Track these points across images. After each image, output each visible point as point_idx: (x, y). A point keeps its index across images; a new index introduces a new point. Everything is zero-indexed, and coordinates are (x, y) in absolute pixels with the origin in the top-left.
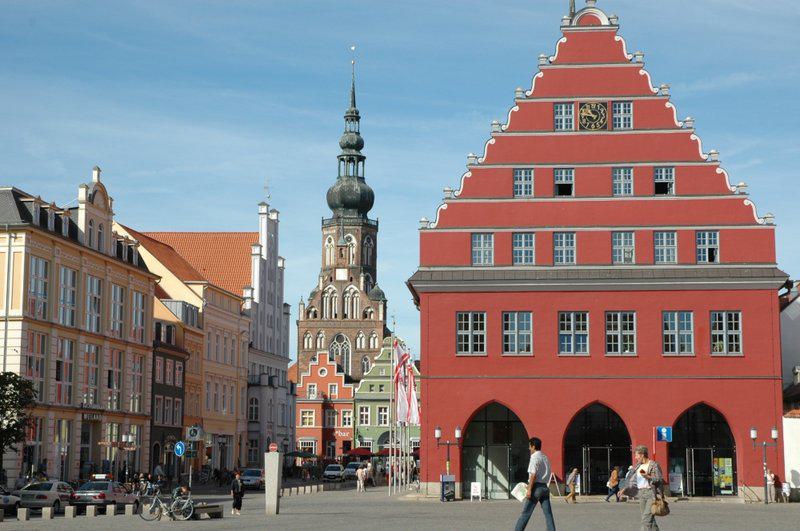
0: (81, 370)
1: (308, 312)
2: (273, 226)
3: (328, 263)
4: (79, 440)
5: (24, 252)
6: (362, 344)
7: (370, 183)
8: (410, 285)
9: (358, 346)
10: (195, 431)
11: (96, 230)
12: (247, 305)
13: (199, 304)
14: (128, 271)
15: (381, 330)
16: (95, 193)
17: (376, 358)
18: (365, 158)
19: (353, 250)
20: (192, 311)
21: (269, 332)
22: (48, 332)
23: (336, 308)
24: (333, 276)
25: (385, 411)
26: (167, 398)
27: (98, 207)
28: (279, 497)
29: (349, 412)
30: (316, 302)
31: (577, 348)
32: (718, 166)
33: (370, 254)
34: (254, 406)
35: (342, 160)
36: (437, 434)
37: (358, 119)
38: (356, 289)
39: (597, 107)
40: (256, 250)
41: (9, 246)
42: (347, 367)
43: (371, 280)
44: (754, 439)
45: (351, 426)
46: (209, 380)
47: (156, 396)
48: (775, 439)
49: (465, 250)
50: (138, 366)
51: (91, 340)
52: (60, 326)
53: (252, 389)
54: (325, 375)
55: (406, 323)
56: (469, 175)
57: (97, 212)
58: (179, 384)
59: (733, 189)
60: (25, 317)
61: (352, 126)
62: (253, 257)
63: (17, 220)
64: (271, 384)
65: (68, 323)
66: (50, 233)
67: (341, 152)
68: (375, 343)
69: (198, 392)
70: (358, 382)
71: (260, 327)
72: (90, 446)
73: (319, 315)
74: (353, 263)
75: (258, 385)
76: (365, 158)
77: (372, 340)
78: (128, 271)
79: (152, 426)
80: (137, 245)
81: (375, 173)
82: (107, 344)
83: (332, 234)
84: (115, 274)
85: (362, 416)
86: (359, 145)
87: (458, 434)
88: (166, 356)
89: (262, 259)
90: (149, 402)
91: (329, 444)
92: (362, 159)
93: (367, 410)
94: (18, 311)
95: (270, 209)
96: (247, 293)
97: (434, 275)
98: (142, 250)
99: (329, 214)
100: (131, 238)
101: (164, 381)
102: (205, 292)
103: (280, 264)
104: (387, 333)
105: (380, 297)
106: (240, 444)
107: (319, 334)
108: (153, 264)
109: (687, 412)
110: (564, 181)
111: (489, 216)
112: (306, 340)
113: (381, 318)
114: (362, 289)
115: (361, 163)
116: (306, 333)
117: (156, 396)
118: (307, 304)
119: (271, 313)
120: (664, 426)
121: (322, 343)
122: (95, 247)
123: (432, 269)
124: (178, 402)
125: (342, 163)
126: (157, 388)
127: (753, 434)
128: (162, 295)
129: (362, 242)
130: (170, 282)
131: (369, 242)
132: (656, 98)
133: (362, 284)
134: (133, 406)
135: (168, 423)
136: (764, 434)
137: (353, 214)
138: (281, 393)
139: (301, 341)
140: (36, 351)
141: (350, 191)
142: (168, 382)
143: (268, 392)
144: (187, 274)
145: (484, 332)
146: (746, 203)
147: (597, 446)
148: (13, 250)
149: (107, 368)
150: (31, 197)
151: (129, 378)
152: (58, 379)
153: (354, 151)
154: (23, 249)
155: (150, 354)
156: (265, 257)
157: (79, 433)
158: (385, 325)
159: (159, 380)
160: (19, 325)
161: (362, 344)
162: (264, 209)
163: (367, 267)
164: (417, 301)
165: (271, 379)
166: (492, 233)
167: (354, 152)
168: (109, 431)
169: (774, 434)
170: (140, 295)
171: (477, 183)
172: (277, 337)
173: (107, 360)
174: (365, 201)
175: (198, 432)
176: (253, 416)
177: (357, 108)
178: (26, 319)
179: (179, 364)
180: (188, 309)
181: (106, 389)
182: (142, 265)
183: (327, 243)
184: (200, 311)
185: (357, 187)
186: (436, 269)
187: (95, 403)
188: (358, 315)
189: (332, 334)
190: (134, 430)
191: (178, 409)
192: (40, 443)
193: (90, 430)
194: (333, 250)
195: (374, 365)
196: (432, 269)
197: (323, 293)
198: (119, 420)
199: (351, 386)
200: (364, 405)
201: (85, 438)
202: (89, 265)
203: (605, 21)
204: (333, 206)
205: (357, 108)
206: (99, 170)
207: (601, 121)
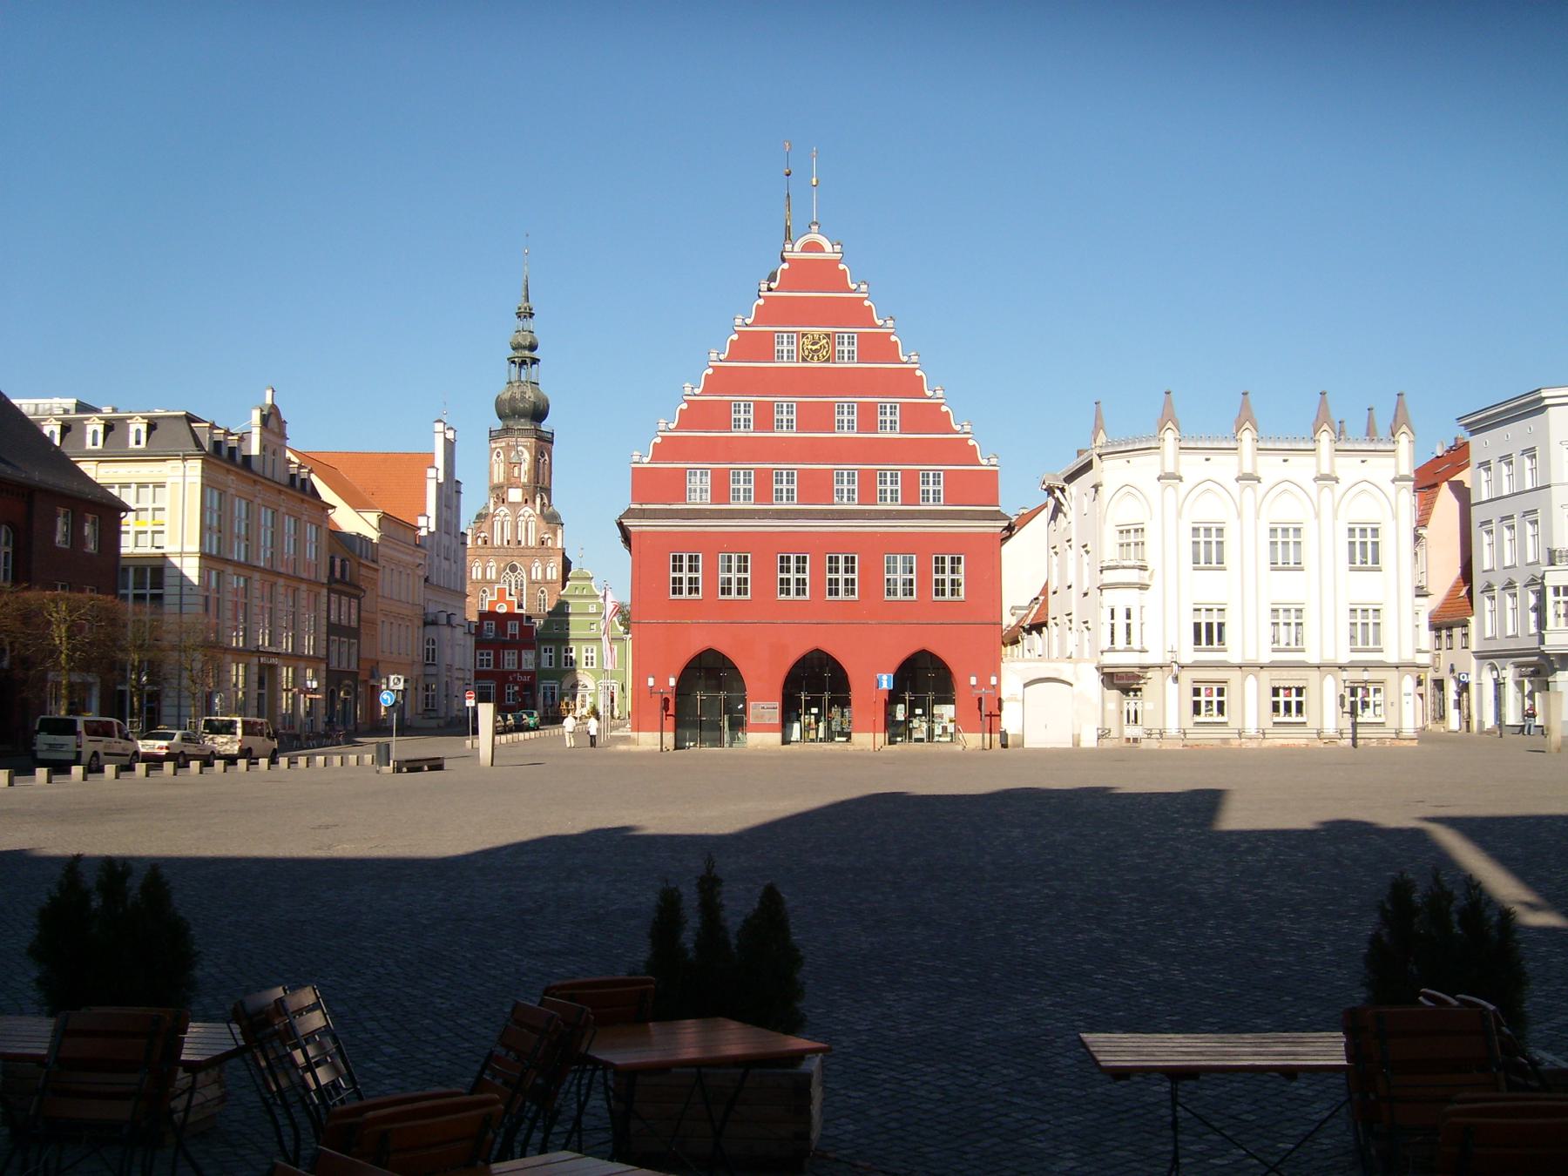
0: (229, 605)
2: (450, 446)
4: (256, 685)
6: (537, 574)
7: (545, 389)
8: (620, 525)
12: (423, 532)
19: (525, 467)
21: (445, 564)
23: (507, 536)
36: (651, 682)
49: (676, 485)
50: (267, 594)
51: (239, 571)
53: (430, 629)
57: (271, 437)
58: (354, 624)
63: (192, 449)
64: (449, 624)
67: (512, 353)
71: (436, 560)
75: (434, 623)
79: (328, 670)
81: (549, 380)
87: (672, 682)
88: (341, 593)
96: (422, 521)
98: (313, 477)
99: (498, 424)
105: (552, 520)
108: (326, 494)
109: (943, 663)
111: (706, 451)
122: (268, 475)
127: (973, 681)
134: (308, 646)
135: (344, 666)
136: (984, 682)
137: (525, 424)
143: (446, 631)
144: (358, 503)
145: (699, 575)
148: (188, 480)
151: (256, 610)
153: (525, 355)
155: (324, 592)
157: (256, 678)
162: (439, 427)
169: (993, 681)
171: (695, 415)
174: (539, 413)
177: (531, 303)
179: (354, 603)
181: (229, 623)
182: (315, 493)
188: (532, 542)
191: (354, 650)
205: (531, 303)
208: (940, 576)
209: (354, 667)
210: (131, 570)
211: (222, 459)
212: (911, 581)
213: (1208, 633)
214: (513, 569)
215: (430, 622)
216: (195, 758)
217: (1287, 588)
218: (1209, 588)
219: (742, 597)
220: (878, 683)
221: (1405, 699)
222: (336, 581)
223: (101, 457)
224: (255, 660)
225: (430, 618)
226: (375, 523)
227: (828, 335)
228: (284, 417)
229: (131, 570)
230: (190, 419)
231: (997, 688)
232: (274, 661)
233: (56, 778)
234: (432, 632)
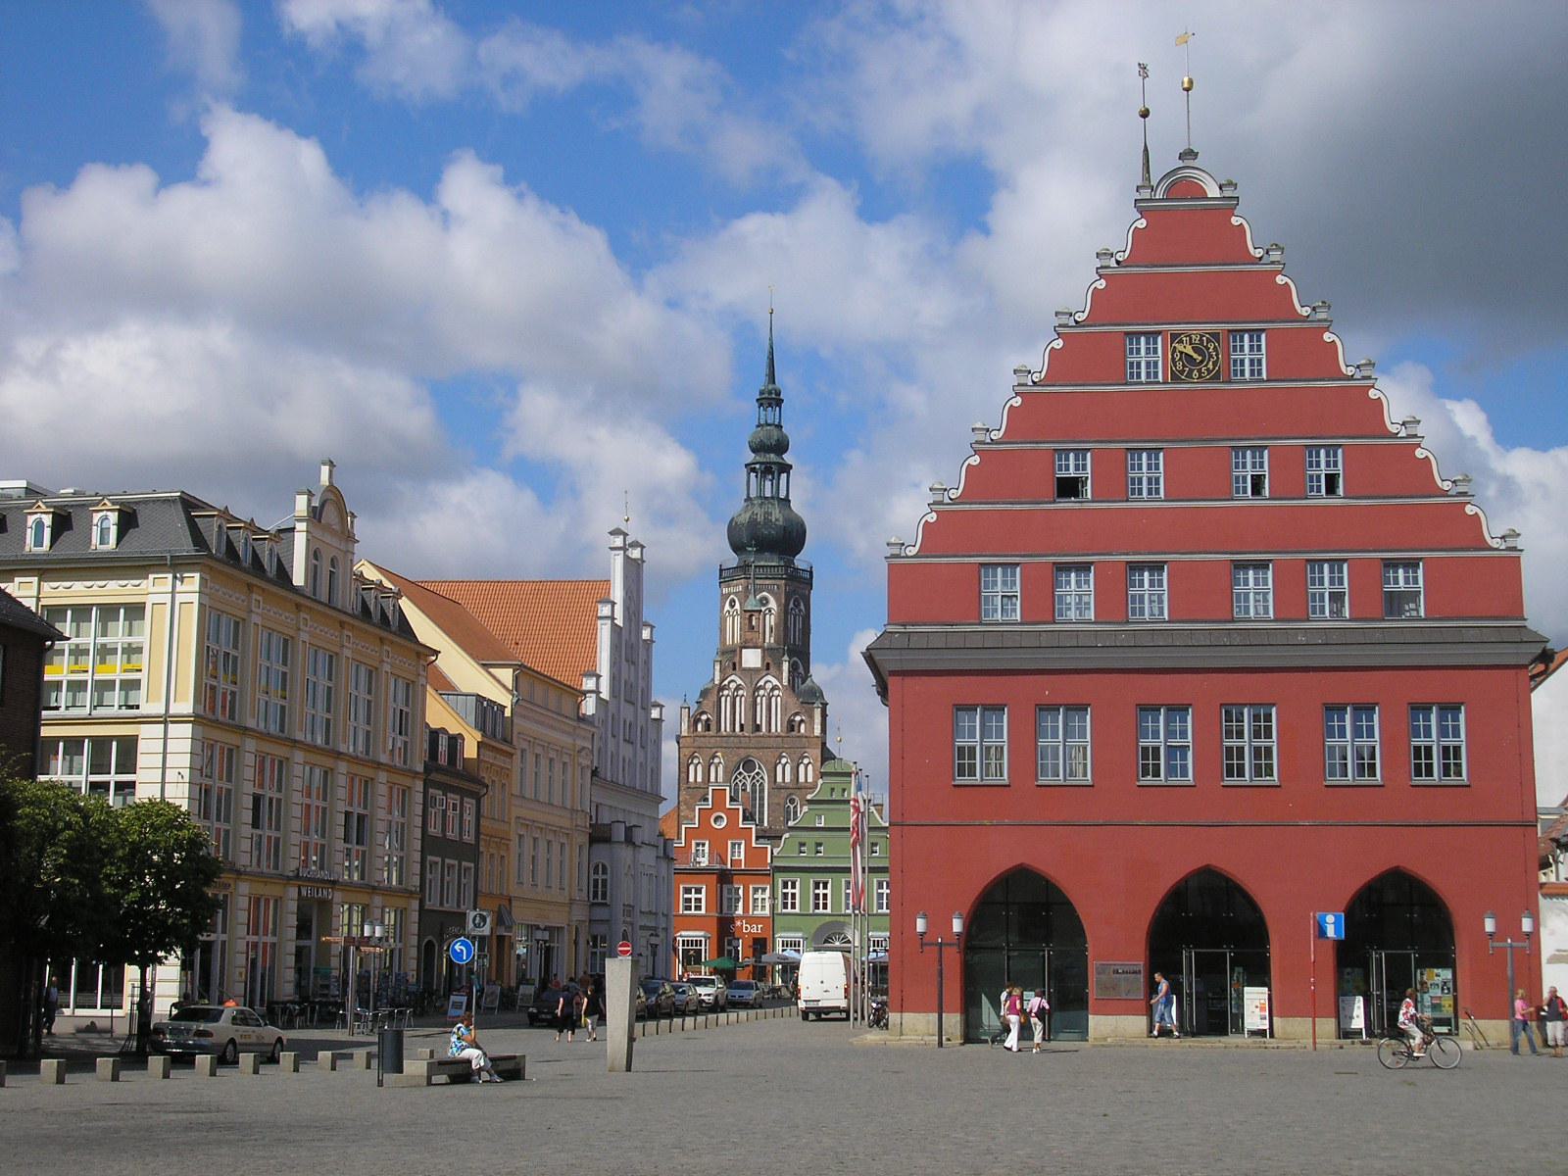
0: (297, 811)
1: (697, 721)
3: (729, 642)
4: (293, 933)
5: (196, 606)
6: (784, 774)
9: (779, 779)
10: (483, 919)
11: (325, 568)
13: (505, 700)
14: (382, 640)
15: (818, 752)
16: (323, 505)
17: (809, 797)
19: (771, 621)
20: (495, 714)
21: (626, 751)
22: (332, 767)
23: (741, 716)
24: (737, 660)
25: (825, 887)
27: (328, 528)
28: (631, 1039)
29: (764, 890)
30: (708, 705)
31: (1171, 771)
32: (1419, 445)
33: (799, 625)
34: (600, 877)
35: (754, 470)
36: (921, 925)
37: (779, 402)
38: (775, 682)
39: (1201, 340)
40: (605, 610)
41: (173, 593)
42: (761, 813)
43: (801, 670)
44: (1491, 935)
45: (767, 912)
46: (550, 837)
47: (429, 858)
48: (1528, 934)
49: (971, 584)
52: (261, 733)
54: (724, 824)
55: (861, 728)
56: (975, 460)
58: (469, 838)
59: (1446, 486)
60: (196, 715)
61: (771, 415)
62: (599, 622)
63: (186, 547)
64: (629, 840)
65: (274, 729)
66: (245, 571)
67: (751, 457)
68: (808, 773)
69: (502, 853)
70: (781, 837)
71: (611, 742)
72: (311, 943)
73: (713, 727)
74: (770, 640)
75: (607, 840)
76: (791, 467)
77: (802, 768)
78: (382, 640)
80: (398, 595)
82: (343, 767)
83: (736, 594)
84: (353, 646)
85: (785, 895)
86: (781, 447)
87: (957, 926)
88: (446, 788)
89: (614, 626)
90: (417, 868)
91: (730, 944)
92: (786, 468)
93: (794, 887)
94: (185, 706)
95: (629, 540)
96: (589, 684)
97: (914, 638)
98: (405, 604)
99: (732, 559)
100: (387, 584)
101: (444, 830)
102: (516, 679)
103: (646, 634)
104: (827, 756)
105: (810, 697)
106: (576, 943)
107: (714, 757)
110: (1072, 473)
112: (692, 768)
113: (817, 731)
114: (785, 683)
116: (692, 757)
118: (694, 707)
119: (630, 718)
120: (1329, 911)
121: (718, 774)
122: (324, 598)
123: (910, 629)
124: (467, 869)
125: (753, 475)
126: (429, 845)
127: (1489, 925)
128: (446, 688)
129: (787, 605)
130: (456, 664)
131: (797, 605)
132: (1306, 325)
133: (785, 675)
135: (447, 907)
138: (647, 856)
139: (684, 770)
140: (267, 785)
141: (767, 521)
142: (449, 834)
143: (625, 854)
144: (486, 654)
146: (1470, 510)
147: (1207, 941)
148: (179, 598)
149: (342, 807)
150: (214, 508)
152: (256, 824)
153: (770, 456)
154: (195, 598)
155: (419, 785)
156: (619, 622)
158: (824, 744)
159: (432, 830)
160: (186, 730)
161: (784, 774)
162: (619, 541)
163: (794, 647)
164: (883, 691)
165: (629, 830)
166: (1018, 564)
167: (772, 457)
168: (345, 921)
169: (1527, 925)
170: (363, 669)
172: (640, 758)
173: (342, 793)
175: (488, 920)
176: (599, 894)
177: (778, 384)
178: (197, 720)
180: (486, 712)
183: (727, 607)
184: (508, 713)
185: (775, 433)
187: (322, 868)
188: (778, 726)
189: (736, 759)
190: (390, 918)
192: (224, 937)
193: (312, 919)
194: (737, 619)
195: (805, 809)
196: (910, 629)
197: (721, 688)
198: (364, 899)
200: (789, 877)
201: (304, 929)
202: (309, 632)
203: (1213, 191)
204: (737, 547)
206: (331, 464)
207: (1210, 366)
208: (1234, 742)
211: (231, 559)
214: (748, 765)
215: (599, 836)
216: (204, 1050)
219: (1366, 780)
220: (1321, 932)
222: (439, 769)
223: (44, 569)
224: (293, 892)
226: (509, 681)
227: (1215, 336)
230: (189, 504)
231: (1534, 937)
232: (324, 894)
233: (264, 1069)
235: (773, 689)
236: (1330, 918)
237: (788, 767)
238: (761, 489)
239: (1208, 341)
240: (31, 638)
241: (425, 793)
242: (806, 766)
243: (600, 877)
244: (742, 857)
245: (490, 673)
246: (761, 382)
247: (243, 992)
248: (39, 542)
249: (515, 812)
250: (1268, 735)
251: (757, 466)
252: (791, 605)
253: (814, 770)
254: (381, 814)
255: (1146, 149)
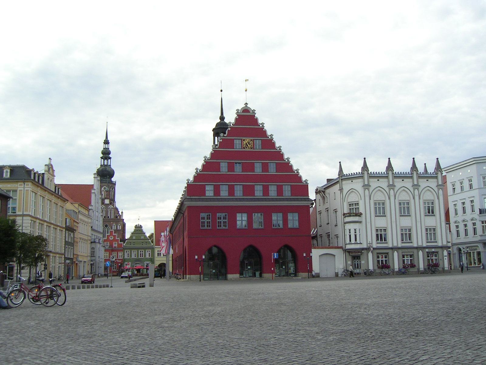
18: (111, 158)
26: (69, 247)
33: (113, 194)
37: (109, 143)
38: (113, 207)
47: (66, 246)
49: (201, 191)
67: (102, 155)
75: (95, 242)
76: (111, 158)
77: (118, 226)
90: (64, 248)
92: (110, 158)
93: (142, 252)
115: (109, 160)
117: (66, 246)
123: (192, 197)
127: (305, 255)
143: (98, 245)
155: (64, 230)
159: (67, 240)
186: (193, 197)
191: (72, 251)
196: (192, 197)
199: (122, 243)
207: (251, 146)
209: (72, 257)
210: (484, 222)
212: (210, 222)
213: (381, 237)
217: (406, 222)
218: (381, 223)
221: (445, 258)
225: (93, 241)
228: (54, 169)
229: (484, 222)
234: (93, 245)
235: (112, 208)
236: (275, 254)
237: (115, 226)
238: (104, 163)
239: (250, 141)
240: (4, 198)
241: (65, 232)
242: (119, 226)
243: (93, 250)
244: (117, 246)
245: (73, 205)
246: (105, 138)
247: (453, 243)
248: (6, 175)
249: (80, 236)
250: (210, 219)
251: (104, 158)
252: (111, 189)
253: (121, 227)
254: (58, 236)
255: (222, 98)
